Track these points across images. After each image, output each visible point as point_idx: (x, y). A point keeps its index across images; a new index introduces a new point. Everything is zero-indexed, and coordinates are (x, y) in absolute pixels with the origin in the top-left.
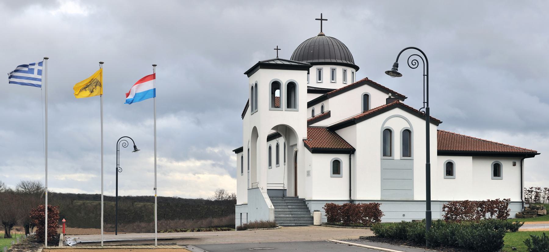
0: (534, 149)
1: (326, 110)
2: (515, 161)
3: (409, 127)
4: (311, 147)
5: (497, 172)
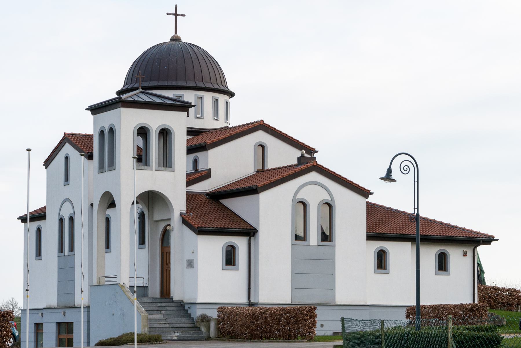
1: (201, 167)
3: (330, 199)
4: (197, 226)
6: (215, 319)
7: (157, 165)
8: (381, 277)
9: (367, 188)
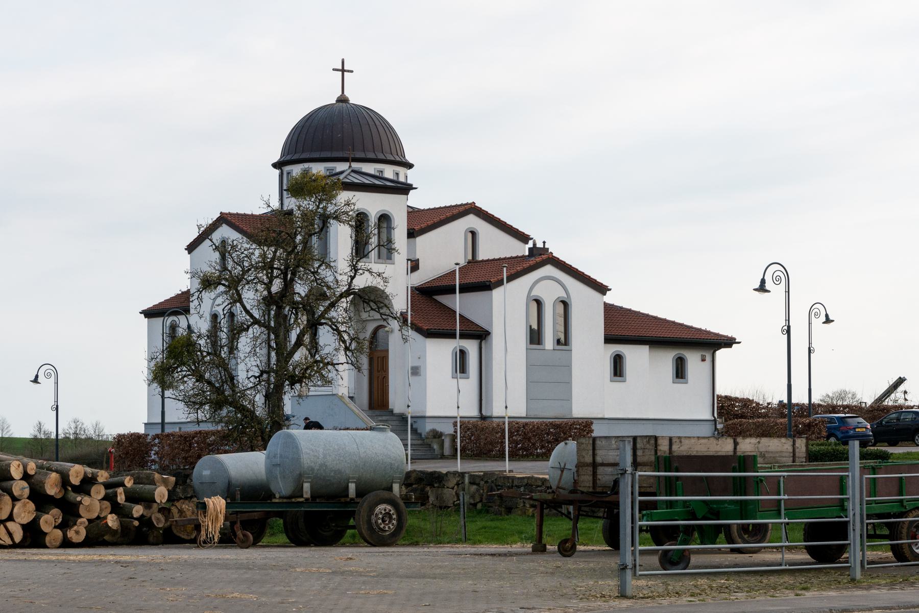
2: (704, 354)
3: (566, 296)
5: (680, 372)
6: (450, 435)
7: (377, 257)
8: (618, 386)
9: (605, 283)
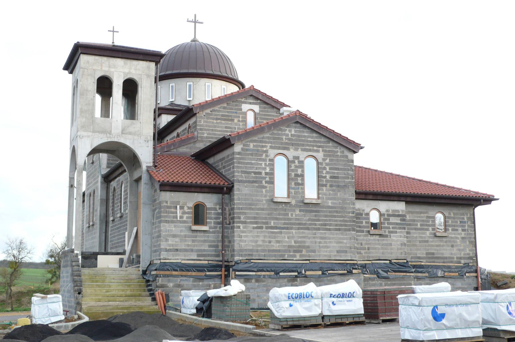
0: (489, 193)
